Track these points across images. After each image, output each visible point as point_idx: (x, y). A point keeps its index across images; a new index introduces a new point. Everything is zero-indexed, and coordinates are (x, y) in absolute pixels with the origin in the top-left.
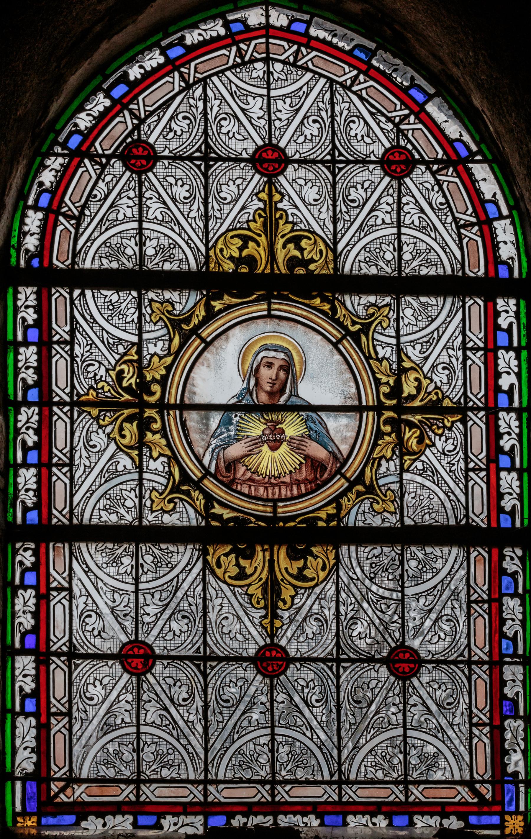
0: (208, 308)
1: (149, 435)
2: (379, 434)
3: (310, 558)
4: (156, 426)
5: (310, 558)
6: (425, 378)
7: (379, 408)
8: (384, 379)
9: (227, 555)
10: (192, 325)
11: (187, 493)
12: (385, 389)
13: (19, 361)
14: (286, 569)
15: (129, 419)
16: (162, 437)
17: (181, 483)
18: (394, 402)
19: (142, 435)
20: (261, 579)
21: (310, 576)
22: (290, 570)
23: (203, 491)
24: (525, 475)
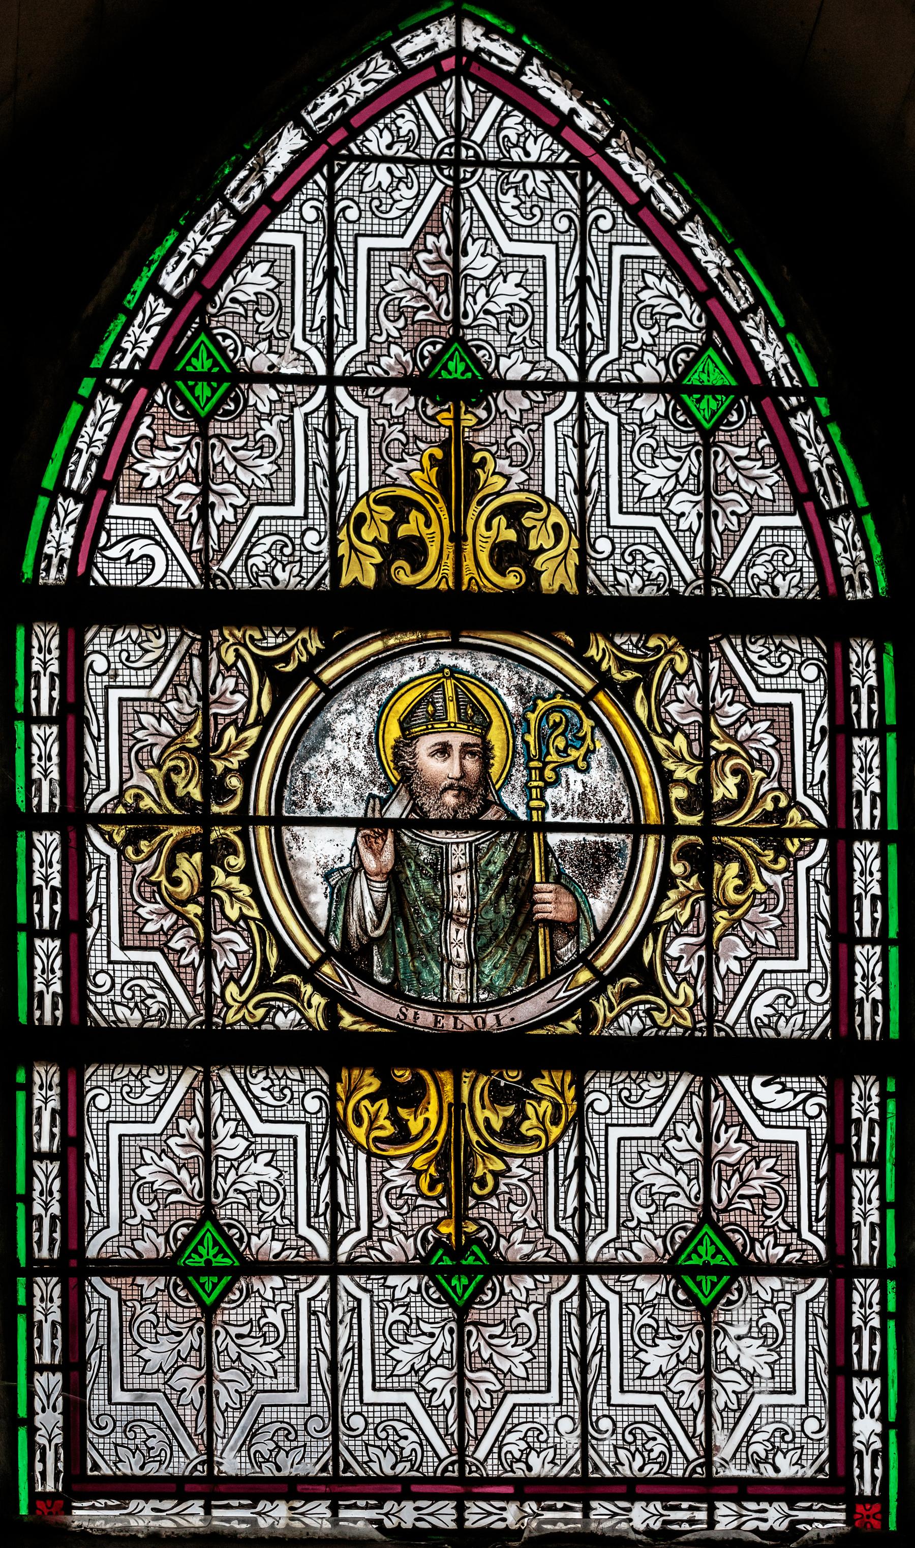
0: (590, 1019)
1: (692, 777)
3: (385, 539)
4: (237, 862)
5: (385, 539)
7: (669, 829)
8: (680, 773)
9: (541, 550)
12: (237, 862)
13: (738, 876)
15: (185, 846)
16: (671, 772)
17: (282, 970)
20: (480, 503)
21: (531, 1133)
22: (422, 519)
23: (321, 988)
24: (20, 708)
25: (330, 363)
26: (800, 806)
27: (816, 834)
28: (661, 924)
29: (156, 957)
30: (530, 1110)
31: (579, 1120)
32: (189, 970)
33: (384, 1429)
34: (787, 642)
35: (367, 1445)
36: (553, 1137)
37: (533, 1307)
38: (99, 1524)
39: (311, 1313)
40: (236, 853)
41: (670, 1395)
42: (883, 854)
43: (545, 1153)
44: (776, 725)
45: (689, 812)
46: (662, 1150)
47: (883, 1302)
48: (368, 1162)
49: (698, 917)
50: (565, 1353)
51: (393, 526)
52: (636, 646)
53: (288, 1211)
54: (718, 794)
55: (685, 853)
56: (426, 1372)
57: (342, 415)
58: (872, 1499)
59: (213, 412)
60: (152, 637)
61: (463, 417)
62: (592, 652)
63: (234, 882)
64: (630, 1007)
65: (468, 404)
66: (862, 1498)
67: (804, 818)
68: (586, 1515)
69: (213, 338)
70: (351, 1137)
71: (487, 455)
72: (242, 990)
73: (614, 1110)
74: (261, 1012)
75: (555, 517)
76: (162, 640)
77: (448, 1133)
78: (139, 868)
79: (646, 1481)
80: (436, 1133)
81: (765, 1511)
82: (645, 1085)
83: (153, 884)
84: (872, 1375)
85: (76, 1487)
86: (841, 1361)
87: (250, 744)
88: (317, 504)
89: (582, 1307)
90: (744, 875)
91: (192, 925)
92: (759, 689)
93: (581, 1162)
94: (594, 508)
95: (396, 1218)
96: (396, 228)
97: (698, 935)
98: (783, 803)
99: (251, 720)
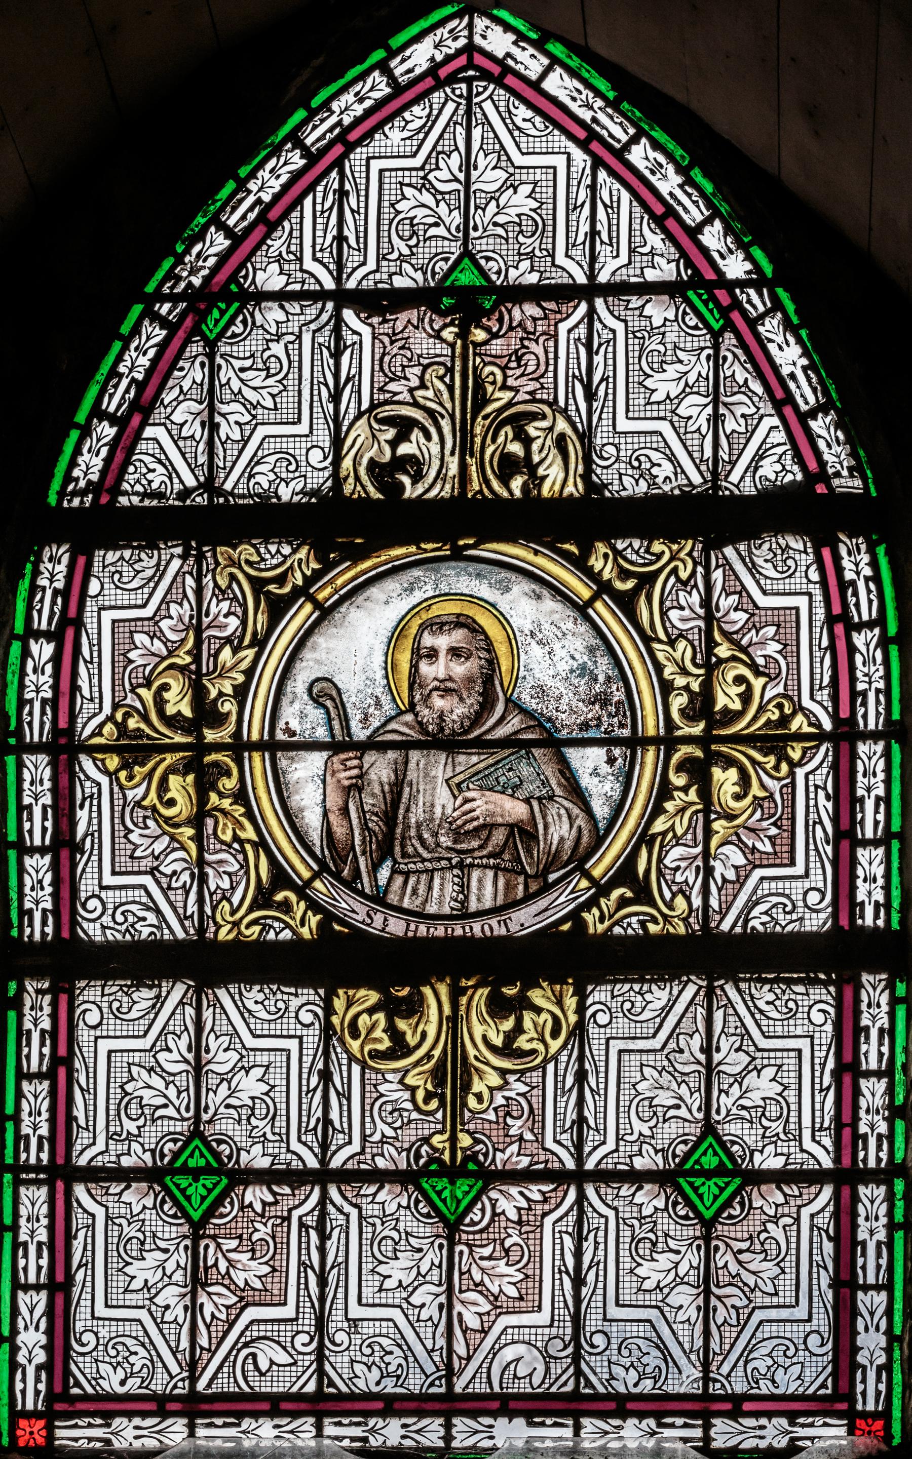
1: (214, 797)
2: (665, 791)
4: (229, 784)
6: (154, 809)
9: (371, 1011)
10: (287, 589)
11: (624, 574)
12: (229, 784)
14: (428, 437)
15: (730, 717)
18: (208, 759)
19: (202, 800)
21: (527, 1047)
23: (314, 906)
25: (581, 1197)
26: (106, 772)
27: (821, 737)
28: (249, 646)
29: (147, 880)
30: (527, 1024)
31: (580, 1031)
32: (180, 892)
33: (369, 1346)
34: (119, 937)
35: (352, 1361)
36: (552, 1051)
37: (395, 255)
38: (83, 1444)
39: (301, 1225)
40: (229, 774)
41: (666, 1309)
42: (887, 754)
43: (543, 1067)
44: (129, 852)
45: (216, 764)
46: (666, 1063)
47: (890, 1214)
48: (363, 1074)
49: (209, 655)
50: (362, 211)
51: (519, 1029)
52: (271, 927)
53: (280, 1123)
54: (721, 701)
55: (219, 720)
56: (415, 1289)
57: (570, 1144)
58: (875, 1415)
59: (221, 334)
60: (143, 556)
61: (447, 1145)
62: (314, 920)
63: (226, 803)
64: (283, 562)
65: (440, 1161)
66: (865, 1415)
67: (103, 761)
68: (577, 1433)
69: (698, 1215)
70: (573, 425)
71: (424, 1108)
72: (675, 571)
73: (304, 451)
74: (257, 929)
75: (355, 1045)
76: (154, 561)
77: (445, 1050)
78: (780, 689)
79: (641, 1397)
80: (433, 1047)
81: (763, 1427)
82: (648, 997)
83: (763, 674)
84: (877, 1288)
85: (59, 1407)
86: (845, 1276)
87: (244, 665)
88: (322, 421)
89: (579, 1222)
90: (744, 781)
91: (726, 635)
92: (764, 592)
93: (336, 398)
94: (315, 1056)
95: (390, 1132)
96: (408, 149)
97: (209, 637)
98: (123, 775)
99: (246, 642)
